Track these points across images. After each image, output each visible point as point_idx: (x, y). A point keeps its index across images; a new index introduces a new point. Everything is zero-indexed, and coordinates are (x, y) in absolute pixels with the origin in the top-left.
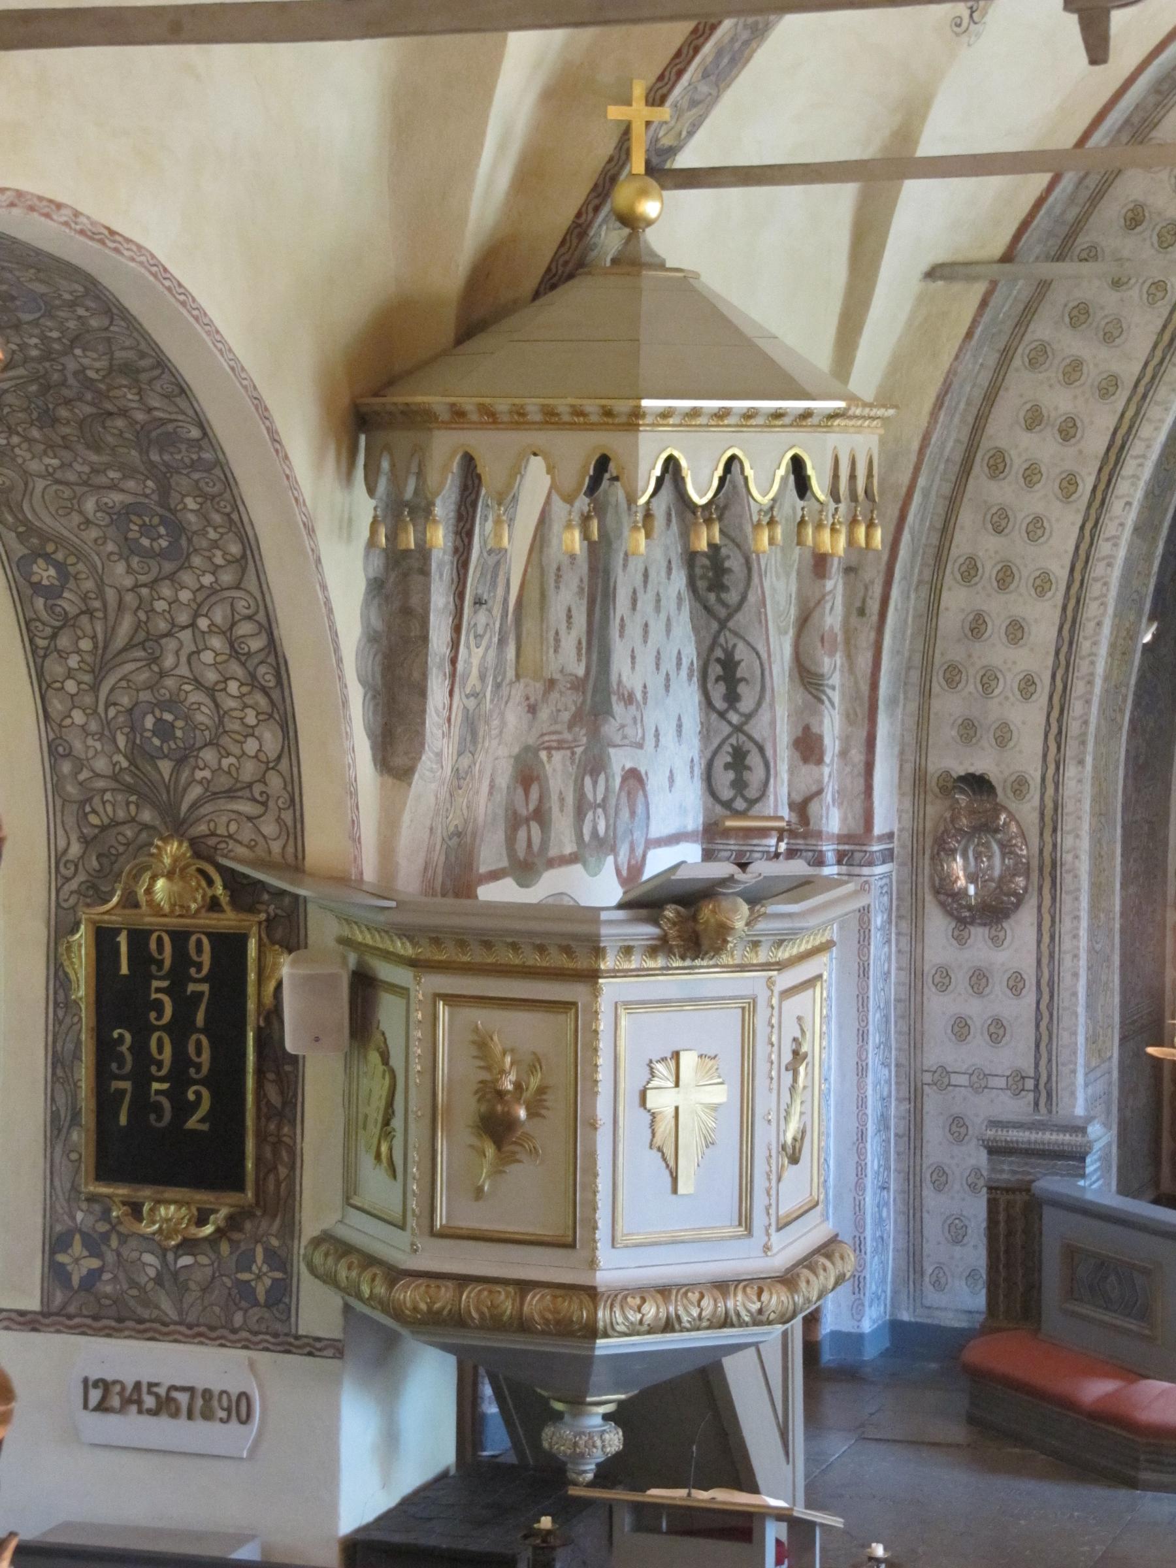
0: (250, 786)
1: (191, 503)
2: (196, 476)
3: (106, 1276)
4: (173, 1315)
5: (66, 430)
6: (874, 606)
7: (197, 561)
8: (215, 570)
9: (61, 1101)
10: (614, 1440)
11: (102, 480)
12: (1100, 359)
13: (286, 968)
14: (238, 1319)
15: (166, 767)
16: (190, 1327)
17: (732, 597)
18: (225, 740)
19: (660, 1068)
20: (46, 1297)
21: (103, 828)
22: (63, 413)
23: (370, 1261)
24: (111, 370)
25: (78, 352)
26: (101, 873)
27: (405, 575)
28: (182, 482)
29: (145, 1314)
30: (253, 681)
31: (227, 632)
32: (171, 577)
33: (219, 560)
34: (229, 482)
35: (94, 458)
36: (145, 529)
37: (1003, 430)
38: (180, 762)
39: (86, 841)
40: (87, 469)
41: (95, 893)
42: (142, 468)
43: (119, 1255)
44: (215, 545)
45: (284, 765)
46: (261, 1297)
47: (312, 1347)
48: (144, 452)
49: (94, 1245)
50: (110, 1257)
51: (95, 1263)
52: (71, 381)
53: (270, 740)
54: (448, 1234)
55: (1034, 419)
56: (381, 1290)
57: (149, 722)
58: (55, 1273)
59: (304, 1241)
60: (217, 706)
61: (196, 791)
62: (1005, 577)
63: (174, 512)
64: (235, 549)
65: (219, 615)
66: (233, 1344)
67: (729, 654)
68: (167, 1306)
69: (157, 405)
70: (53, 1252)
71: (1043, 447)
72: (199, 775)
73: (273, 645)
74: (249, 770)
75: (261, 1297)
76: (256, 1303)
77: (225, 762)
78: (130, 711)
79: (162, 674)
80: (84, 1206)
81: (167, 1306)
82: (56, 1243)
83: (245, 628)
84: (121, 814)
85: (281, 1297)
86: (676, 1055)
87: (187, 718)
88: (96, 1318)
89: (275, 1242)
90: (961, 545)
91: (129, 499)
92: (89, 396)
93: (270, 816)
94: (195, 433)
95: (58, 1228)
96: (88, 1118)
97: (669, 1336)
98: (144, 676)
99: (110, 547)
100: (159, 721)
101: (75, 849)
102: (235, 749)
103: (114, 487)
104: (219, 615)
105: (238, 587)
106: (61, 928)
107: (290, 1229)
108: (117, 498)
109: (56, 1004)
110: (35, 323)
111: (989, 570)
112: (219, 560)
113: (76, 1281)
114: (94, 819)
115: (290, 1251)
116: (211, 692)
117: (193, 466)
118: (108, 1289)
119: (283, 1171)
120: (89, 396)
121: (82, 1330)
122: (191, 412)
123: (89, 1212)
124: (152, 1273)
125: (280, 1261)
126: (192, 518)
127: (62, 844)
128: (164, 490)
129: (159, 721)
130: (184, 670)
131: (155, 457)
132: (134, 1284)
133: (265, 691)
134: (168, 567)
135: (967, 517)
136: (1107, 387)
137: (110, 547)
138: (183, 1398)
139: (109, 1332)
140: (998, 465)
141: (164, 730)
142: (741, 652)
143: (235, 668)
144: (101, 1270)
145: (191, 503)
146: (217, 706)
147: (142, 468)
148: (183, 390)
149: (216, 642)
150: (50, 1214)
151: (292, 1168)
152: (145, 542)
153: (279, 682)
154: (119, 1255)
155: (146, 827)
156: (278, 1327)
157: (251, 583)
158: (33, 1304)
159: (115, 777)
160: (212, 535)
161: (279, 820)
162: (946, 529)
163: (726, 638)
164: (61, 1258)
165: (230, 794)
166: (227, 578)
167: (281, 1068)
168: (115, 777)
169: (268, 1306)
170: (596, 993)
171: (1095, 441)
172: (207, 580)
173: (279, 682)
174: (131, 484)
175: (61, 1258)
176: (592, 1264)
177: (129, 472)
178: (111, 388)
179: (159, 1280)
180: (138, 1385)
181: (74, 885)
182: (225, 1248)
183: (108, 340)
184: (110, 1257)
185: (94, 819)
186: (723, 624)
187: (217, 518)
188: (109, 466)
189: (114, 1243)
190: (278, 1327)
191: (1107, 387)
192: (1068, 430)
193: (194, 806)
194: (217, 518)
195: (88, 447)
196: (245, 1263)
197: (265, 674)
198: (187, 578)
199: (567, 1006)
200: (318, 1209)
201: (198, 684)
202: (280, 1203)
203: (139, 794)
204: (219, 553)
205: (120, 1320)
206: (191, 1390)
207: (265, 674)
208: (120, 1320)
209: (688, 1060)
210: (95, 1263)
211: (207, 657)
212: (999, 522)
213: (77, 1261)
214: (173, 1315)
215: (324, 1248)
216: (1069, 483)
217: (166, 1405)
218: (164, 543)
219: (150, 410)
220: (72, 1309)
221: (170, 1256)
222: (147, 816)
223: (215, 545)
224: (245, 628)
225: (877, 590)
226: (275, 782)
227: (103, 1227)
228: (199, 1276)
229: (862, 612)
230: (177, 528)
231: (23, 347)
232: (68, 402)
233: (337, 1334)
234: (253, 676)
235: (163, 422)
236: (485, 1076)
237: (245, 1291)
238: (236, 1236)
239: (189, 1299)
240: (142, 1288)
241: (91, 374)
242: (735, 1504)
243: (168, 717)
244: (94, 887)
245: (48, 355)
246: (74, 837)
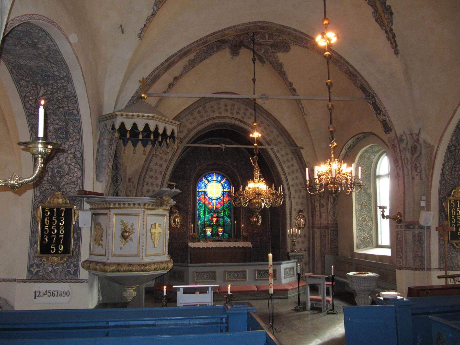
0: (74, 182)
1: (72, 128)
2: (74, 122)
3: (40, 272)
4: (54, 278)
5: (50, 111)
6: (136, 187)
7: (70, 140)
8: (73, 141)
9: (33, 240)
10: (136, 293)
11: (55, 122)
12: (165, 157)
13: (81, 213)
14: (67, 277)
15: (58, 179)
16: (57, 280)
17: (119, 183)
18: (70, 174)
19: (153, 226)
20: (28, 276)
21: (44, 190)
22: (51, 107)
23: (98, 263)
24: (64, 97)
25: (58, 92)
26: (43, 198)
27: (103, 149)
28: (71, 123)
29: (48, 278)
30: (77, 163)
31: (74, 154)
32: (64, 143)
33: (74, 139)
34: (80, 123)
35: (55, 118)
36: (61, 133)
37: (152, 165)
38: (61, 178)
39: (41, 193)
40: (52, 120)
41: (41, 202)
42: (63, 120)
43: (43, 267)
44: (74, 136)
45: (81, 178)
46: (72, 273)
47: (82, 281)
48: (65, 116)
49: (38, 266)
50: (41, 268)
51: (38, 269)
52: (55, 100)
53: (79, 174)
54: (115, 256)
55: (156, 164)
56: (102, 267)
57: (56, 171)
58: (30, 272)
59: (81, 262)
60: (69, 167)
61: (64, 183)
62: (152, 185)
63: (68, 129)
64: (78, 137)
65: (73, 150)
66: (66, 282)
67: (117, 192)
68: (53, 276)
69: (70, 106)
70: (29, 268)
71: (158, 168)
72: (64, 180)
73: (82, 156)
74: (74, 179)
75: (72, 273)
76: (71, 274)
77: (70, 178)
78: (52, 169)
79: (60, 162)
80: (36, 259)
81: (53, 276)
82: (30, 266)
83: (77, 153)
84: (48, 188)
85: (76, 273)
86: (155, 223)
87: (63, 170)
88: (38, 279)
89: (75, 263)
90: (146, 180)
91: (60, 127)
92: (57, 103)
93: (78, 187)
94: (76, 112)
95: (31, 263)
96: (39, 242)
97: (154, 272)
98: (56, 162)
99: (54, 137)
100: (58, 170)
101: (38, 194)
102: (72, 176)
103: (57, 124)
104: (73, 150)
105: (77, 145)
106: (35, 209)
107: (78, 260)
108: (57, 126)
109: (33, 222)
110: (52, 84)
111: (150, 183)
112: (74, 139)
113: (34, 273)
114: (43, 189)
115: (78, 264)
116: (69, 165)
117: (74, 120)
118: (41, 274)
119: (77, 250)
120: (57, 103)
121: (35, 282)
122: (76, 108)
123: (37, 260)
124: (50, 270)
125: (76, 266)
126: (71, 131)
127: (36, 193)
128: (67, 125)
129: (58, 170)
130: (64, 161)
131: (67, 118)
132: (46, 273)
133: (79, 164)
134: (64, 141)
135: (147, 177)
136: (166, 160)
137: (54, 137)
138: (56, 293)
139: (40, 282)
140: (151, 170)
141: (58, 172)
142: (119, 192)
143: (74, 161)
144: (39, 271)
145: (72, 128)
146: (69, 167)
147: (63, 120)
148: (77, 103)
149: (71, 156)
150: (29, 261)
151: (79, 249)
152: (61, 136)
153: (82, 163)
154: (43, 267)
155: (53, 190)
156: (75, 278)
157: (80, 144)
158: (25, 278)
159: (48, 181)
160: (74, 134)
161: (79, 188)
162: (144, 178)
163: (117, 189)
164: (31, 269)
165: (70, 184)
166: (75, 143)
167: (79, 230)
168: (48, 181)
169: (73, 274)
170: (110, 211)
171: (164, 167)
172: (71, 143)
173: (82, 163)
174: (61, 124)
175: (31, 269)
176: (142, 259)
177: (61, 120)
178: (62, 101)
179: (51, 272)
180: (46, 291)
181: (38, 201)
182: (65, 265)
183: (66, 89)
184: (41, 268)
185: (43, 189)
186: (117, 187)
187: (76, 131)
188: (57, 119)
189: (42, 265)
190: (75, 278)
191: (166, 160)
192: (161, 166)
193: (63, 186)
194: (76, 131)
195: (54, 115)
196: (69, 267)
197: (80, 162)
198: (68, 143)
199: (106, 214)
200: (84, 256)
201: (66, 163)
202: (78, 256)
203: (52, 184)
204: (75, 138)
205: (43, 279)
206: (58, 291)
207: (80, 162)
208: (43, 279)
209: (157, 225)
210: (38, 269)
211: (69, 158)
212: (152, 177)
213: (34, 269)
214: (54, 278)
215: (86, 263)
216: (161, 172)
217: (53, 294)
218: (64, 136)
219: (69, 107)
220: (33, 278)
221: (54, 267)
222: (53, 188)
223: (74, 136)
224: (77, 153)
225: (136, 185)
226: (79, 181)
227: (40, 263)
228: (59, 270)
229: (134, 188)
230: (67, 133)
231: (47, 90)
232: (52, 105)
233: (87, 278)
234: (77, 162)
235: (70, 110)
236: (123, 228)
237: (69, 272)
238: (67, 262)
239: (57, 274)
240: (48, 273)
241: (59, 98)
242: (288, 263)
243: (60, 170)
244: (42, 201)
245: (52, 93)
246: (38, 192)
